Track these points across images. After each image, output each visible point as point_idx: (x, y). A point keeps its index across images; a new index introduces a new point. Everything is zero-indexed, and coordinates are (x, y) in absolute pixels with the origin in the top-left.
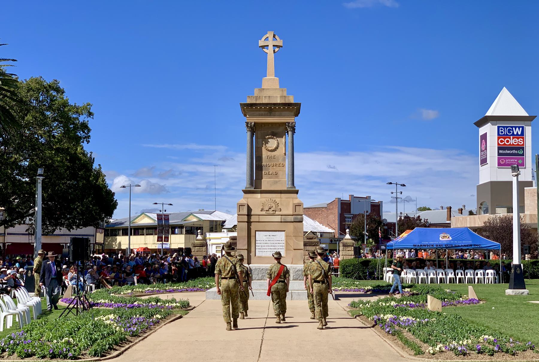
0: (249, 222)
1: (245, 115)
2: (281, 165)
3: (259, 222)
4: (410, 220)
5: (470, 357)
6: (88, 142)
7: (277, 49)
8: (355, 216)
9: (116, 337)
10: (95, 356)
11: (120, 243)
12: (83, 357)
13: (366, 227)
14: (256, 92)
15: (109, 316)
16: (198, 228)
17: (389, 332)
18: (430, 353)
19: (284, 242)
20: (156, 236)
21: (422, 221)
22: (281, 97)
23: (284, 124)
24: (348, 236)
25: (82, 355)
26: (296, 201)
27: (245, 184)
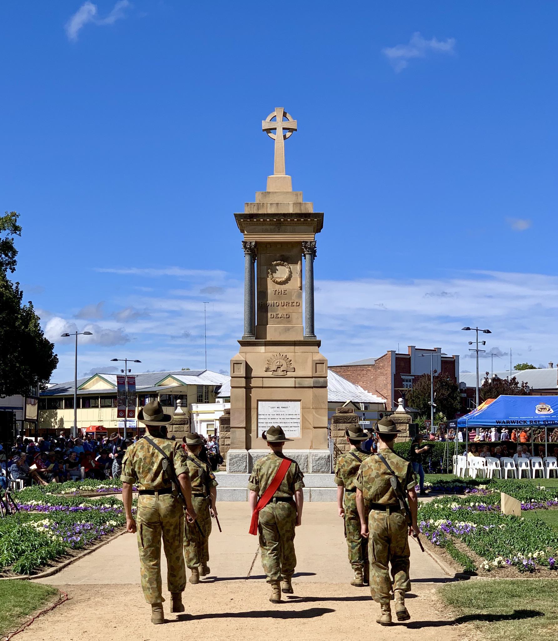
0: (248, 388)
1: (242, 231)
2: (295, 304)
3: (263, 387)
4: (500, 383)
5: (539, 574)
6: (13, 270)
7: (288, 134)
8: (417, 379)
9: (52, 548)
10: (21, 573)
11: (62, 420)
12: (5, 574)
13: (433, 395)
14: (258, 197)
15: (43, 521)
16: (177, 397)
17: (436, 542)
18: (485, 569)
19: (299, 417)
20: (116, 410)
21: (519, 385)
22: (294, 204)
23: (299, 243)
24: (401, 409)
25: (5, 572)
26: (317, 357)
27: (242, 333)
